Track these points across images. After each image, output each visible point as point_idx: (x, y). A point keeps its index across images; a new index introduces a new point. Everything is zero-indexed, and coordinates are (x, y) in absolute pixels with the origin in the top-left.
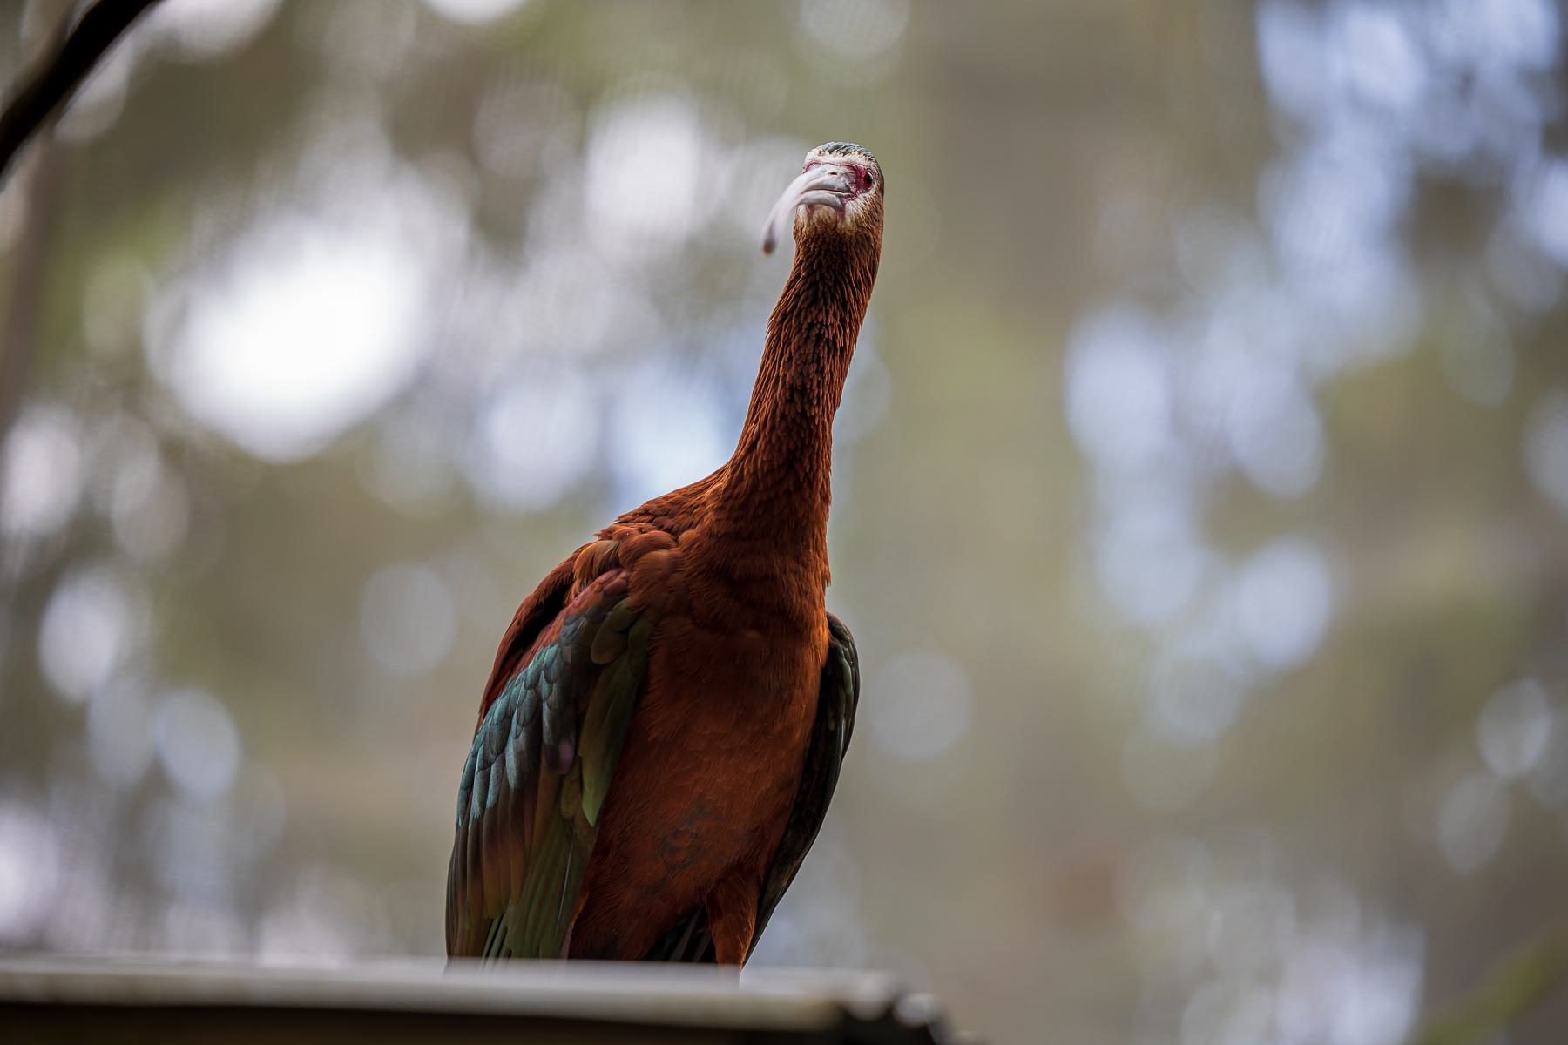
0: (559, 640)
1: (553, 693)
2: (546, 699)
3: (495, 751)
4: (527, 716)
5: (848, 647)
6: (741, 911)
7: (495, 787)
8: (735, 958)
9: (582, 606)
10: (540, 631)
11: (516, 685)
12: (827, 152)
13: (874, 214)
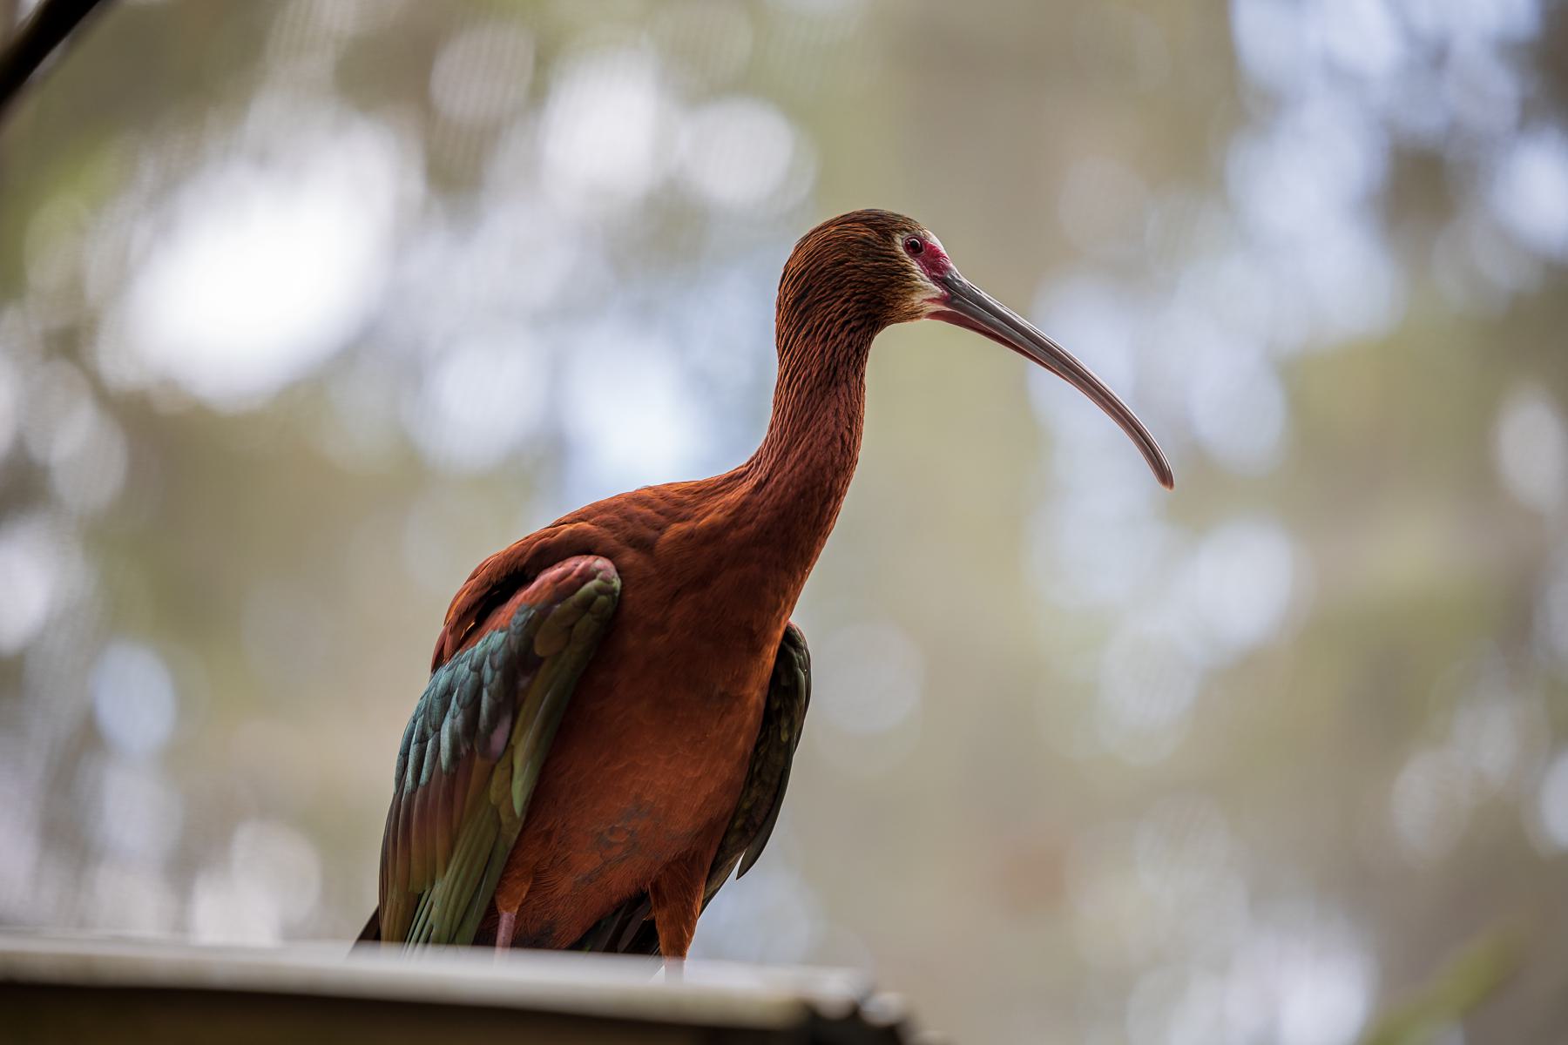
0: (508, 628)
1: (495, 682)
6: (687, 900)
9: (534, 599)
11: (462, 662)
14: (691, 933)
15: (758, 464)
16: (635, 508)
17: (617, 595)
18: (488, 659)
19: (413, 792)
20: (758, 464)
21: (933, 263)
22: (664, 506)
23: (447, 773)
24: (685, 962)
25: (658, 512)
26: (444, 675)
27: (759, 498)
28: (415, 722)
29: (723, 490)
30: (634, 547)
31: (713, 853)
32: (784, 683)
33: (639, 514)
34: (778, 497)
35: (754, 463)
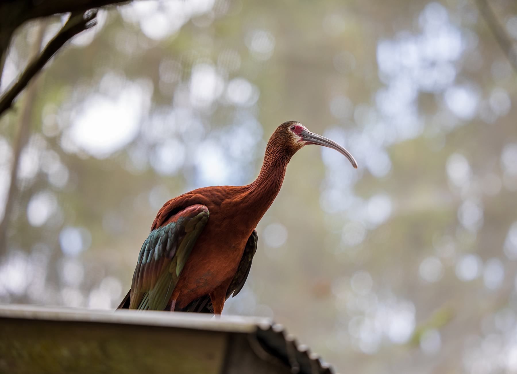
2: (170, 238)
3: (152, 246)
4: (164, 240)
7: (150, 257)
8: (219, 312)
9: (185, 215)
11: (162, 230)
14: (223, 308)
15: (253, 186)
16: (215, 192)
17: (208, 216)
18: (170, 230)
20: (253, 186)
21: (298, 130)
22: (224, 193)
23: (156, 261)
24: (221, 315)
25: (222, 195)
26: (156, 232)
27: (250, 196)
28: (146, 245)
29: (241, 192)
30: (214, 203)
31: (228, 286)
32: (251, 245)
33: (217, 195)
34: (255, 197)
35: (252, 185)
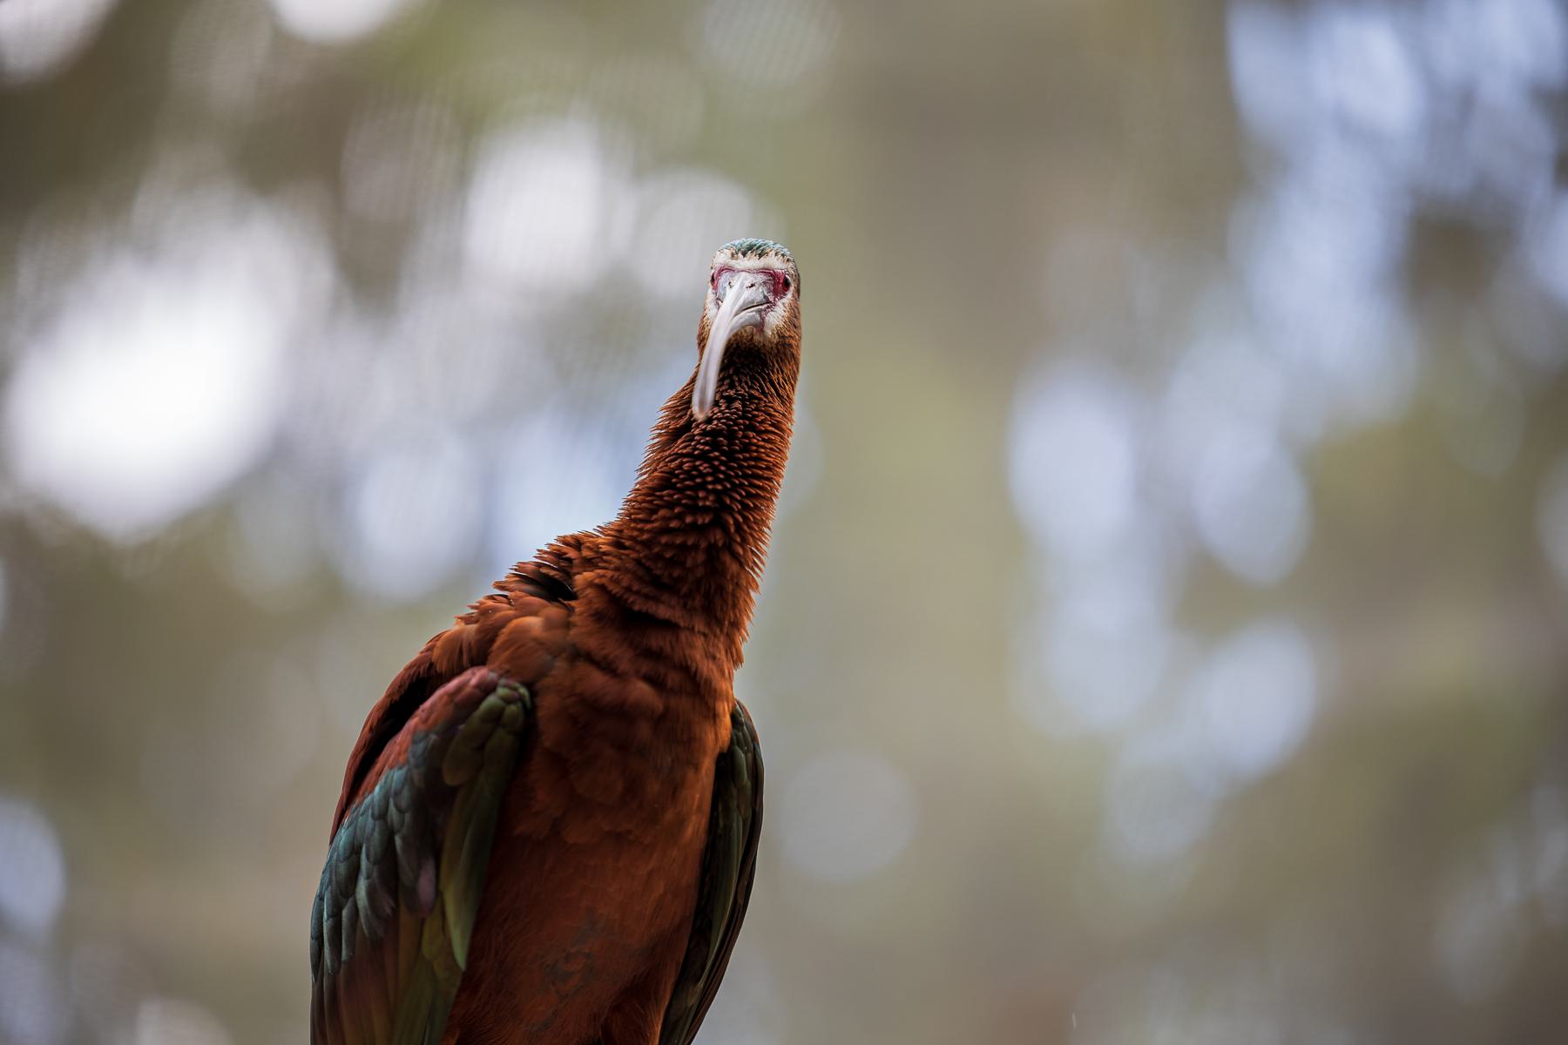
0: (407, 762)
5: (743, 731)
9: (430, 721)
10: (388, 741)
12: (740, 254)
13: (793, 320)
19: (335, 972)
